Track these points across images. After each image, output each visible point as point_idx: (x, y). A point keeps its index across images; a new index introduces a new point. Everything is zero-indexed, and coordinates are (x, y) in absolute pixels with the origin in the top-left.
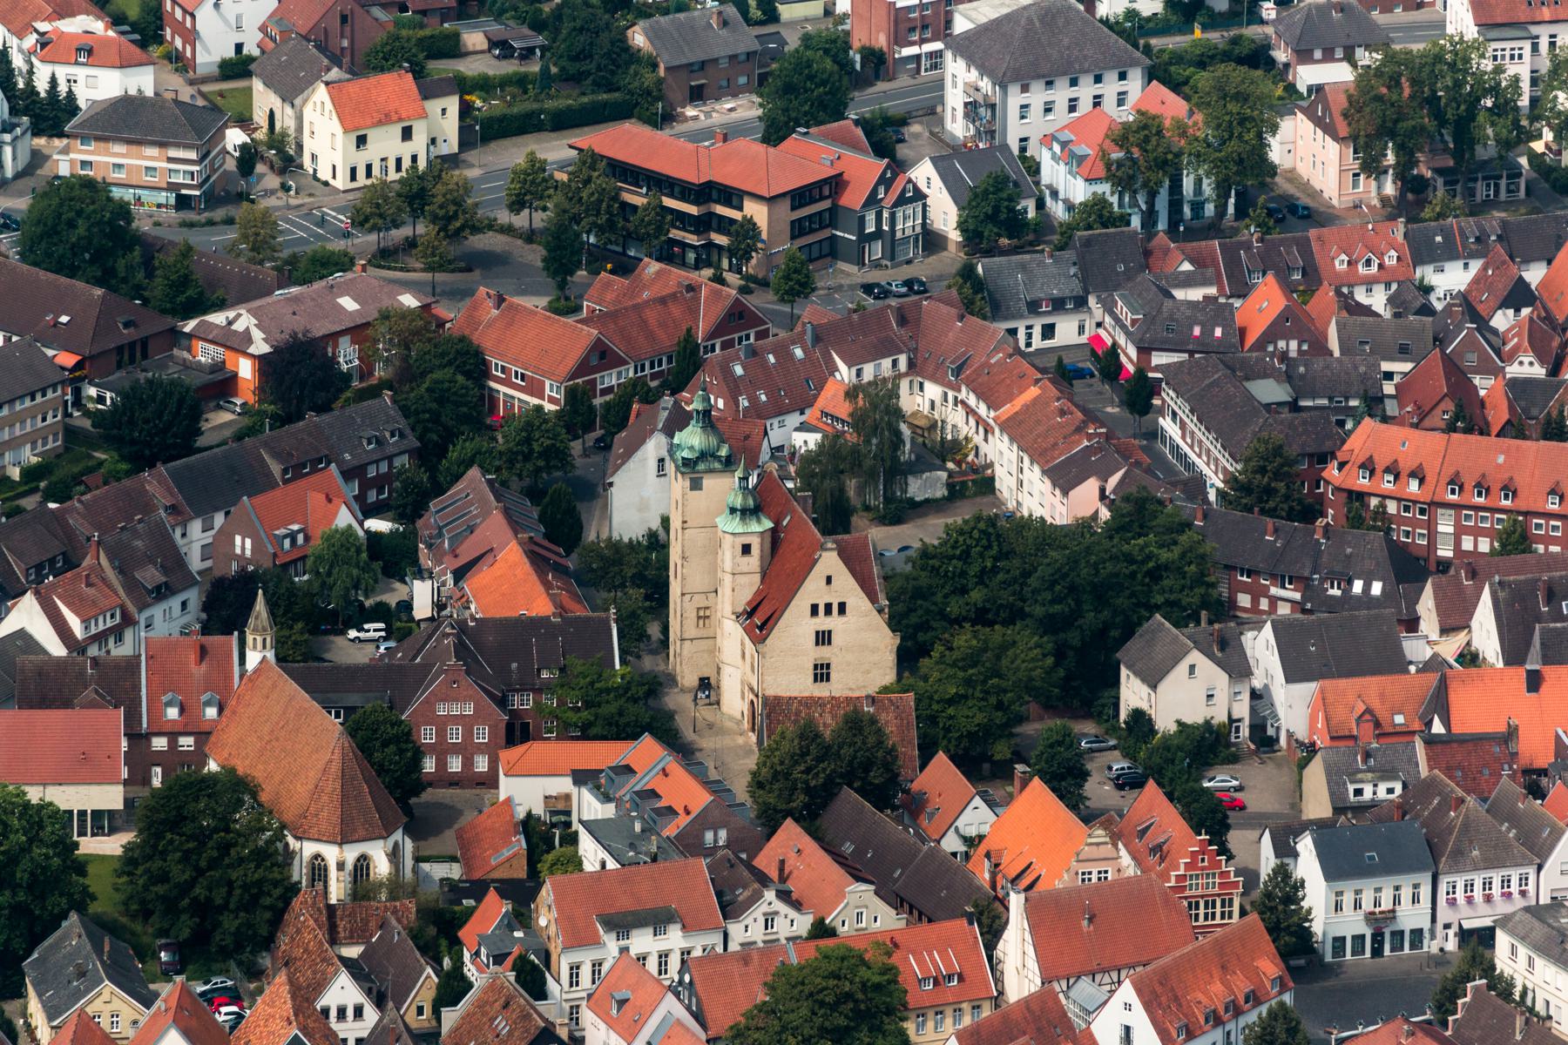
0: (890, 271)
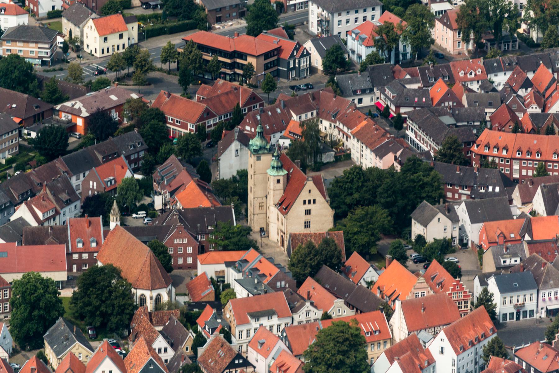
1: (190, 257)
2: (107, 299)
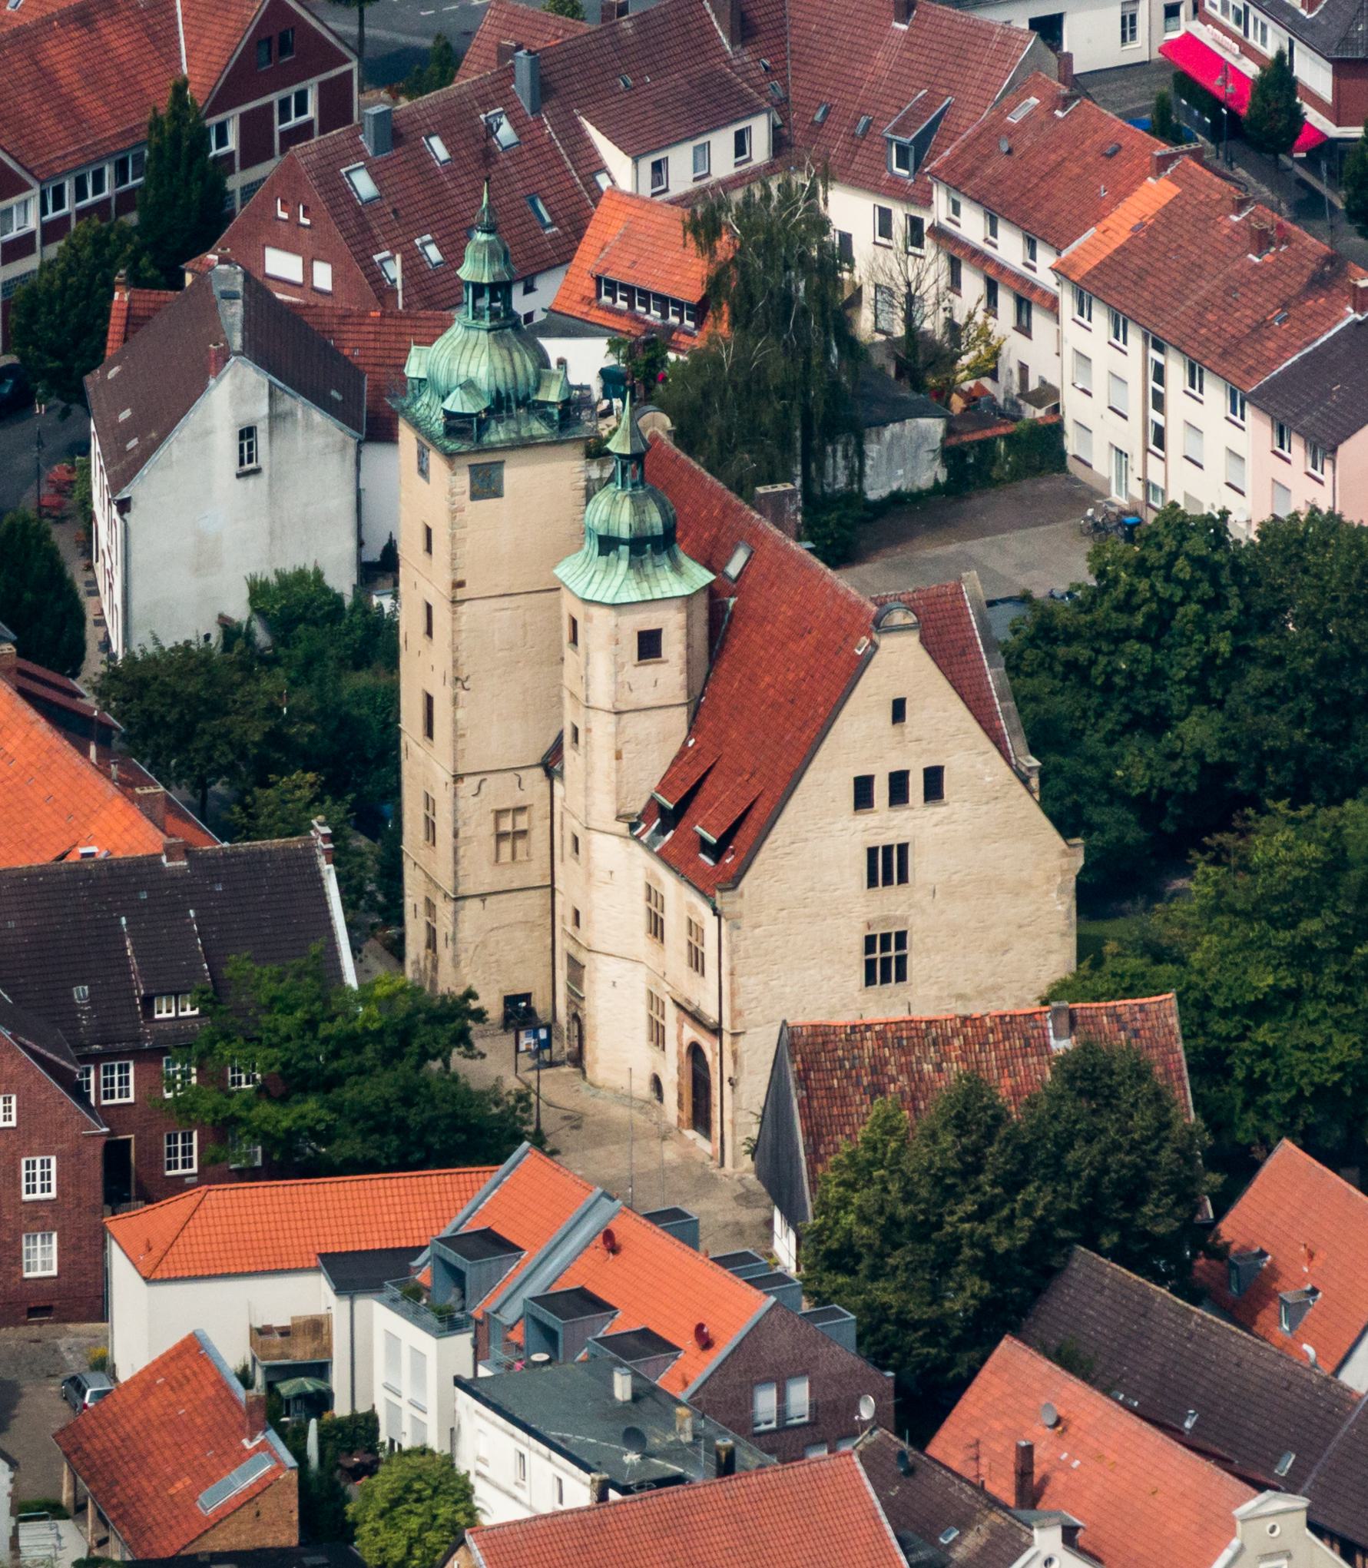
1: (45, 1229)
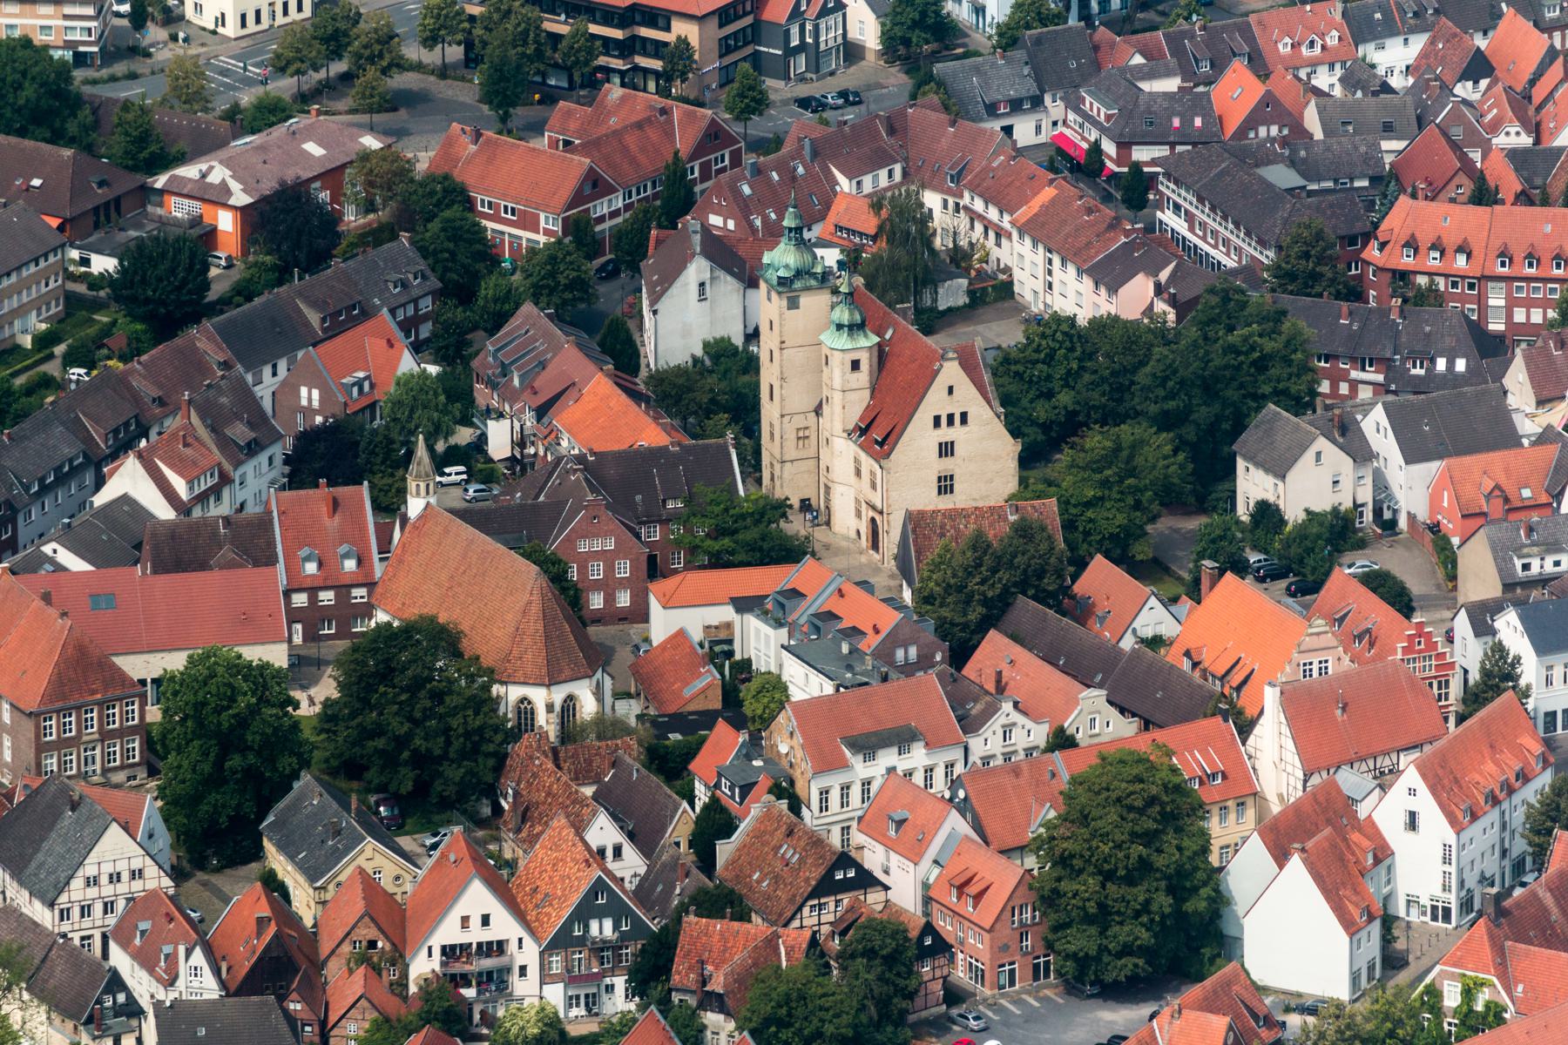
0: (815, 84)
1: (625, 588)
2: (428, 714)
